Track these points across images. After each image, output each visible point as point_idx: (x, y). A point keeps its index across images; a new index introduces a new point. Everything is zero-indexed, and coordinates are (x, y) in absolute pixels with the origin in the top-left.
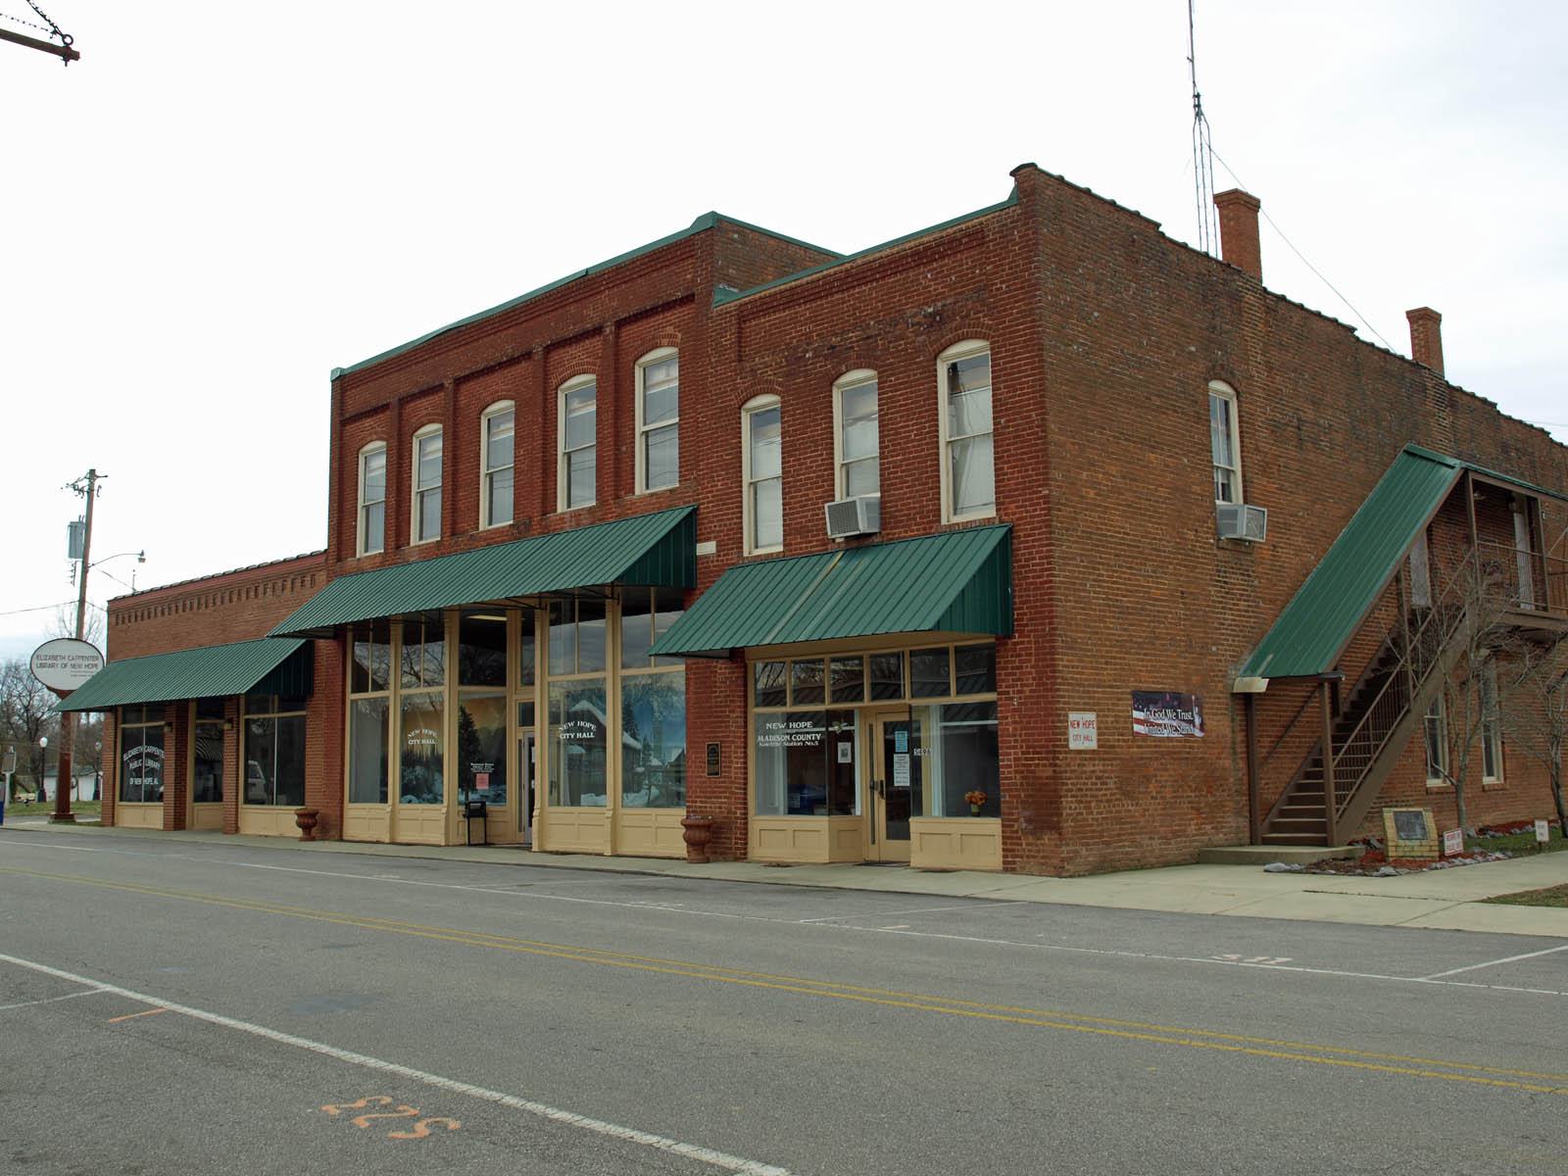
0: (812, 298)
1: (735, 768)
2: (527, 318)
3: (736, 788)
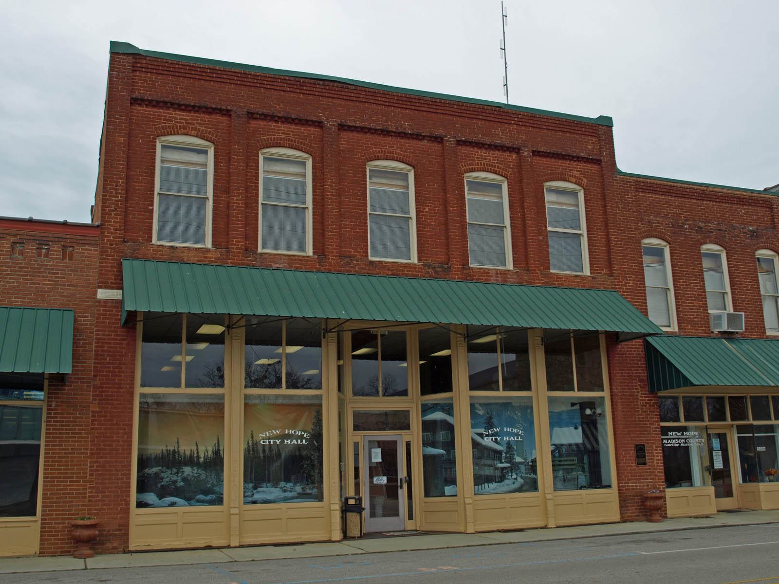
0: (687, 196)
1: (657, 460)
2: (428, 110)
3: (658, 472)
